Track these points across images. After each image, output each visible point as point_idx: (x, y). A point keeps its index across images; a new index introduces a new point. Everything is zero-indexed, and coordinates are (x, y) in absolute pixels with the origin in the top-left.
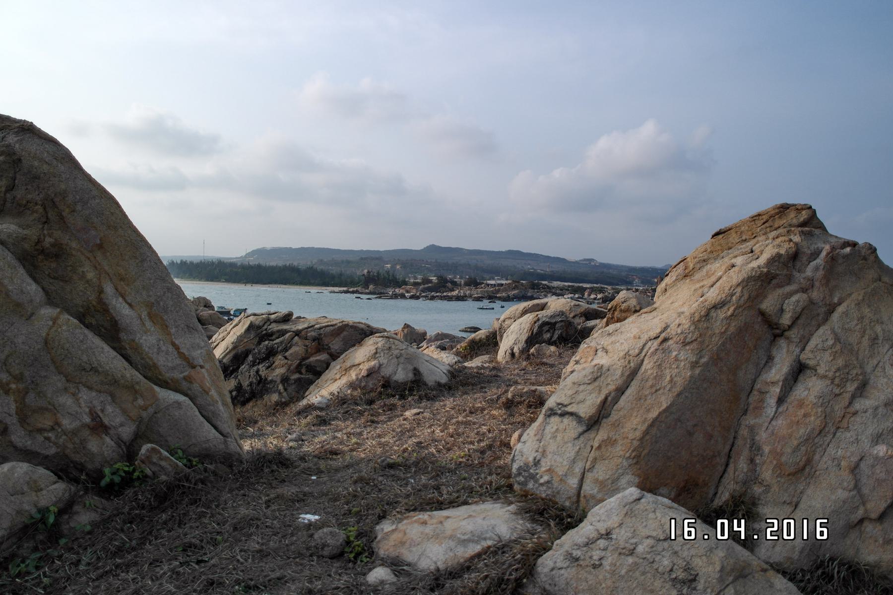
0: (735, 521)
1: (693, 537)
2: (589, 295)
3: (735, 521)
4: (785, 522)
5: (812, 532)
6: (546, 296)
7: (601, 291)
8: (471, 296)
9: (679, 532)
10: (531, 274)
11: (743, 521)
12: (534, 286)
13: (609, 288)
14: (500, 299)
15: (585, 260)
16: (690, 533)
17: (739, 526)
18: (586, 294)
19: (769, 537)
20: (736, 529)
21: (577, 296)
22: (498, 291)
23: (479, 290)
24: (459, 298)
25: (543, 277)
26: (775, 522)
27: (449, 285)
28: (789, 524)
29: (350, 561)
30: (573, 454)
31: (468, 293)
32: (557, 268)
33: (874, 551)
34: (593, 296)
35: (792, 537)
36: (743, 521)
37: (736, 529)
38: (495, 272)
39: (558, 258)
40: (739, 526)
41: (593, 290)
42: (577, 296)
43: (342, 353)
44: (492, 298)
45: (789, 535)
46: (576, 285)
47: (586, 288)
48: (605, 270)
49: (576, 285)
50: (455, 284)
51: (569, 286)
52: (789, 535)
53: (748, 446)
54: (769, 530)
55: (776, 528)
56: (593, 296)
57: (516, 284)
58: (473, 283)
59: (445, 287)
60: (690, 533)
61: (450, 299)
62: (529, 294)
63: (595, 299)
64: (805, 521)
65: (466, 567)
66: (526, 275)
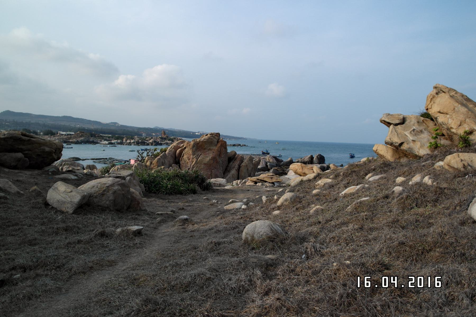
0: (392, 278)
1: (440, 286)
2: (126, 141)
3: (392, 278)
4: (419, 278)
5: (433, 283)
11: (396, 278)
12: (92, 135)
15: (112, 123)
17: (394, 280)
18: (124, 140)
19: (410, 286)
20: (392, 282)
22: (70, 138)
26: (413, 278)
35: (422, 286)
36: (396, 278)
37: (392, 282)
39: (99, 122)
40: (394, 280)
43: (99, 178)
45: (420, 279)
52: (420, 279)
54: (410, 282)
55: (413, 282)
56: (128, 141)
62: (91, 140)
64: (429, 278)
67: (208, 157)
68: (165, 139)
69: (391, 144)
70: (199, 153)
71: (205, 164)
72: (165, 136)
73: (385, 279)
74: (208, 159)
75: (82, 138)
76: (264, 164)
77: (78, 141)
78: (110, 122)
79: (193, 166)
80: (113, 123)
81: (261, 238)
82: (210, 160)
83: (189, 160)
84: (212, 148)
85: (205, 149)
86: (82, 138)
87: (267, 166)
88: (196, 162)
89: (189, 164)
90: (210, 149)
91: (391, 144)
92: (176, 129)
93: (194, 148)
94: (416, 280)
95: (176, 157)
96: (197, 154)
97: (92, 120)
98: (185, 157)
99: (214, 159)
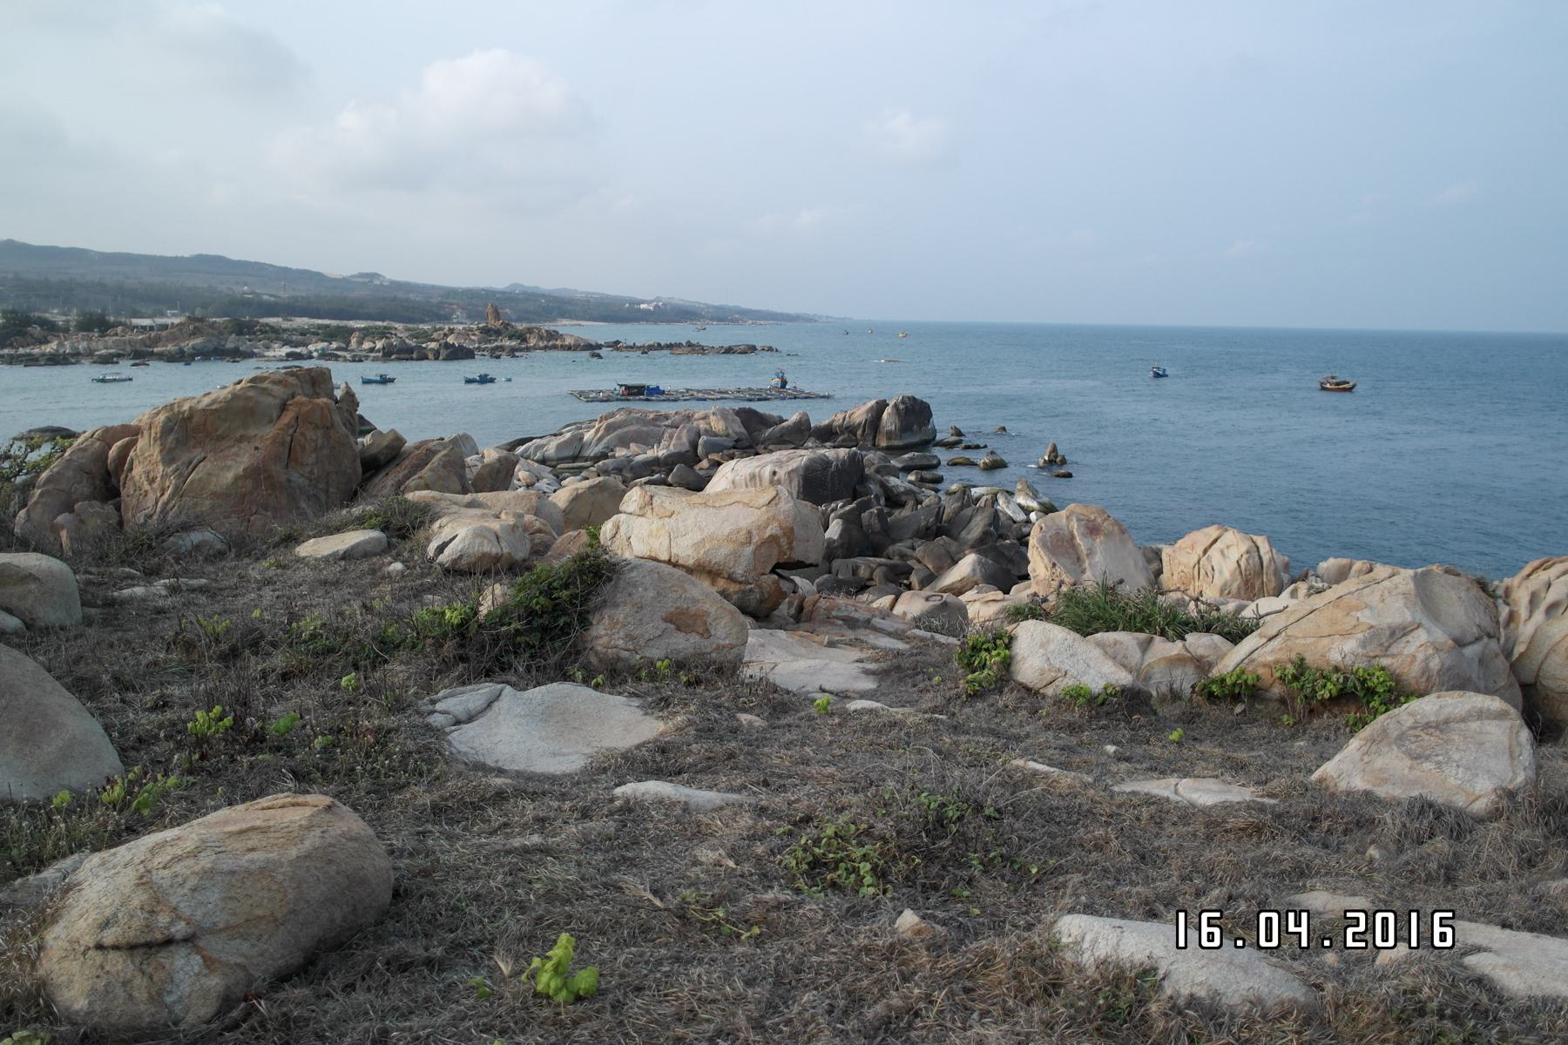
0: (1291, 915)
1: (1449, 943)
2: (360, 343)
3: (1291, 915)
4: (1379, 916)
7: (384, 333)
8: (90, 354)
10: (246, 304)
11: (1304, 915)
12: (242, 329)
13: (399, 326)
14: (161, 357)
16: (1443, 937)
17: (1298, 924)
18: (354, 341)
19: (1350, 943)
20: (1292, 928)
21: (334, 345)
23: (110, 340)
24: (55, 360)
25: (272, 310)
26: (1362, 916)
27: (37, 330)
28: (1385, 920)
31: (82, 346)
32: (303, 291)
34: (367, 345)
36: (1304, 915)
37: (1292, 928)
38: (160, 299)
39: (318, 274)
40: (1298, 924)
41: (366, 333)
42: (334, 345)
44: (141, 356)
46: (334, 323)
47: (354, 330)
48: (401, 295)
49: (334, 323)
50: (51, 328)
51: (320, 327)
54: (1350, 931)
55: (1362, 928)
56: (367, 345)
57: (196, 325)
58: (96, 324)
59: (23, 334)
60: (1443, 937)
61: (31, 361)
62: (230, 345)
63: (372, 350)
66: (234, 305)
67: (229, 468)
68: (498, 333)
70: (198, 453)
71: (215, 495)
72: (498, 324)
74: (230, 476)
75: (198, 341)
76: (685, 439)
77: (182, 351)
78: (355, 272)
79: (166, 504)
80: (367, 275)
82: (237, 479)
83: (152, 481)
84: (252, 432)
85: (221, 438)
86: (198, 341)
87: (694, 446)
88: (177, 488)
89: (152, 497)
90: (241, 440)
93: (171, 438)
94: (1371, 927)
95: (108, 473)
96: (185, 457)
98: (138, 471)
99: (255, 474)
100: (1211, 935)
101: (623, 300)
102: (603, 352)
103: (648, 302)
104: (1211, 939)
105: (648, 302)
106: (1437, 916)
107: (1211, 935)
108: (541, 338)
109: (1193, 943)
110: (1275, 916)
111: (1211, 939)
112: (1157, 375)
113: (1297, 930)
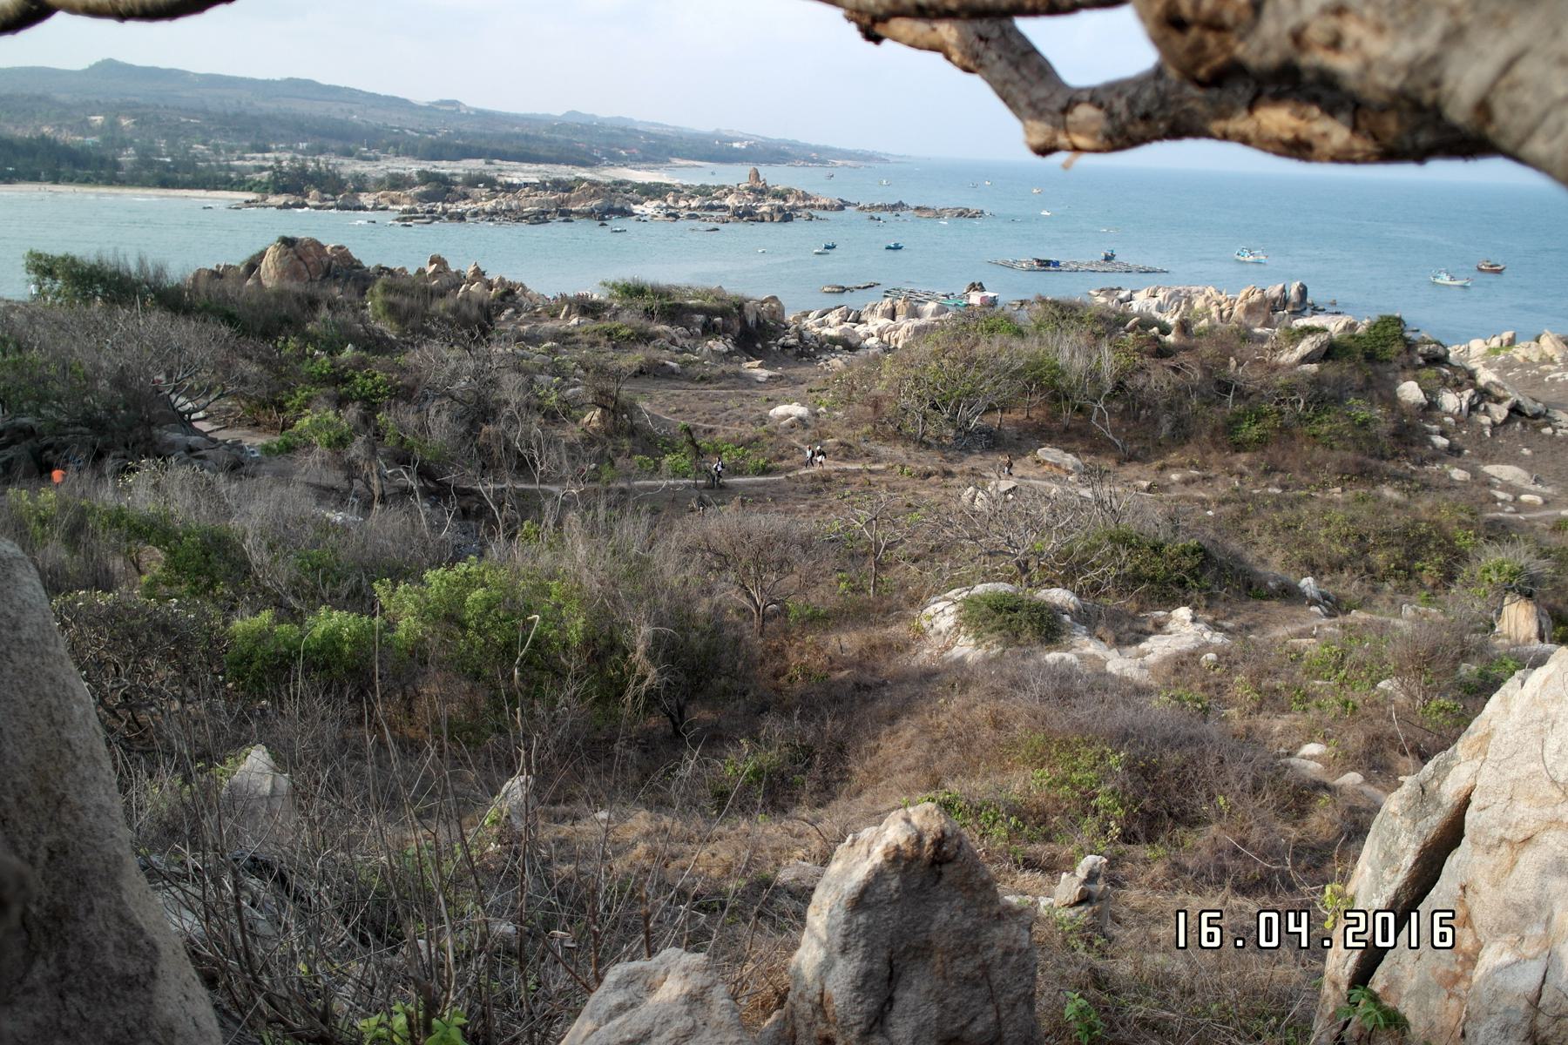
0: (1291, 915)
1: (1216, 943)
3: (1291, 915)
6: (1251, 107)
9: (1193, 936)
11: (1304, 915)
15: (443, 103)
16: (1211, 937)
17: (1298, 924)
20: (1292, 928)
29: (1071, 932)
30: (833, 602)
33: (178, 1042)
36: (1304, 915)
37: (1292, 928)
39: (406, 101)
40: (1298, 924)
43: (122, 183)
45: (1269, 939)
48: (560, 137)
52: (1269, 939)
53: (566, 828)
60: (1211, 937)
65: (1540, 623)
69: (1381, 361)
73: (1269, 920)
81: (223, 174)
91: (1381, 361)
92: (637, 119)
97: (383, 92)
100: (1443, 934)
101: (714, 136)
102: (573, 217)
103: (741, 140)
104: (1443, 940)
105: (741, 140)
106: (1205, 916)
107: (1443, 934)
108: (798, 198)
109: (1425, 946)
110: (1275, 916)
111: (1443, 940)
112: (897, 248)
113: (1297, 930)
